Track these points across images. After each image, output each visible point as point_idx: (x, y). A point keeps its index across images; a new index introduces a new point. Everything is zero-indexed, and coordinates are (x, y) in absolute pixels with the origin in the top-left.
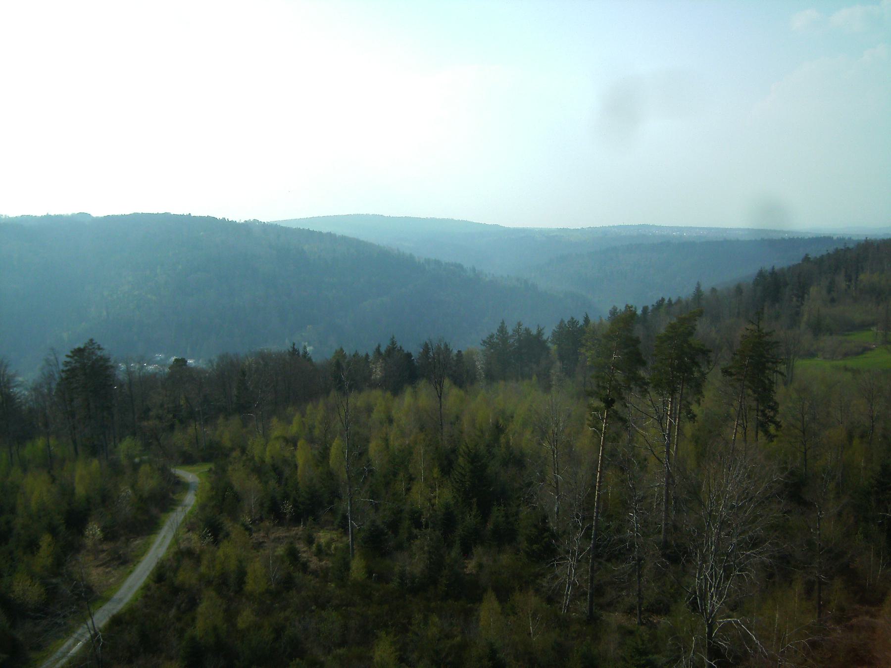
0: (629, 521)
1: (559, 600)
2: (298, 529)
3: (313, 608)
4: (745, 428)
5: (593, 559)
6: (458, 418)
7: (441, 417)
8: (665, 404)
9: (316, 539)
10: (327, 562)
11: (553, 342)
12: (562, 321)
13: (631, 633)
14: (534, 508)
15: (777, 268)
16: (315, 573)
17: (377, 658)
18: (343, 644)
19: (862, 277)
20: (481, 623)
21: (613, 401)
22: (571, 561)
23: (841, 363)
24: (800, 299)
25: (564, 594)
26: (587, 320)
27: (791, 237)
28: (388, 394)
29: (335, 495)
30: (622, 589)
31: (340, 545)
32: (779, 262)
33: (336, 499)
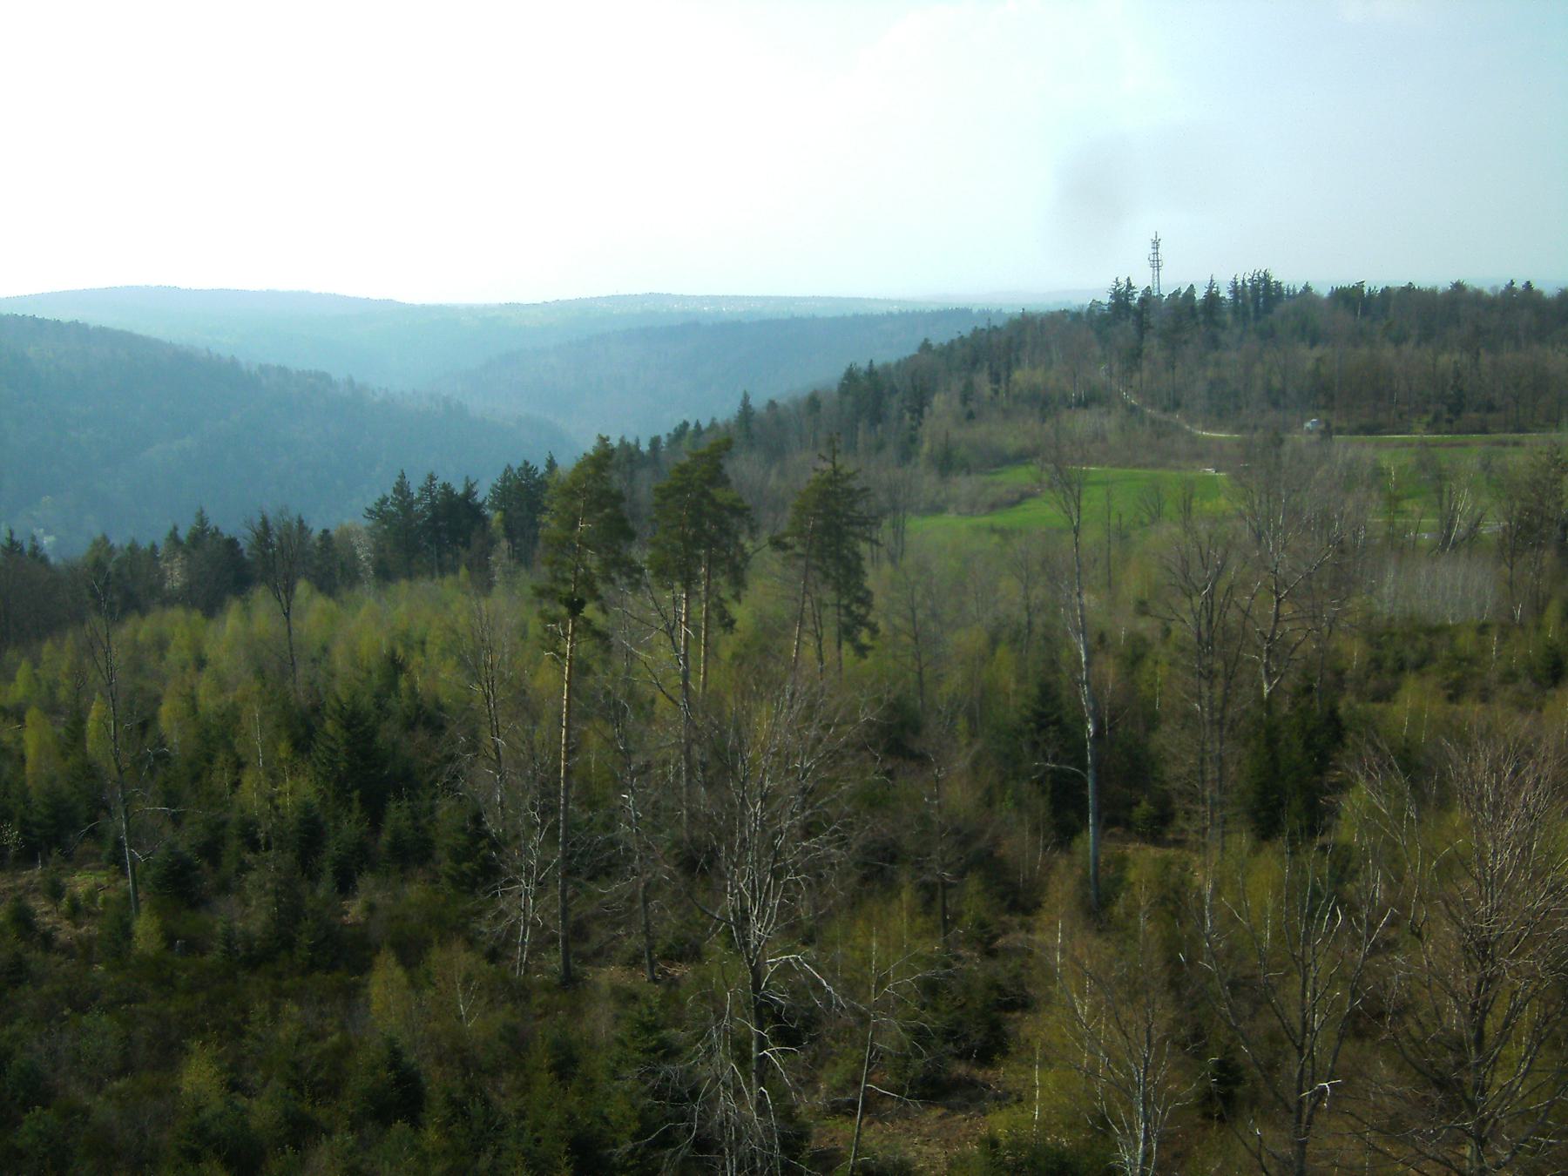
0: (622, 807)
1: (510, 954)
2: (33, 874)
3: (65, 1013)
4: (819, 638)
5: (564, 877)
6: (325, 649)
7: (291, 649)
8: (675, 602)
9: (67, 889)
10: (91, 928)
11: (492, 506)
12: (509, 468)
13: (634, 997)
14: (460, 799)
15: (877, 363)
16: (67, 950)
17: (187, 1088)
18: (126, 1069)
19: (1018, 375)
20: (374, 1007)
21: (582, 603)
22: (525, 885)
23: (985, 520)
24: (916, 415)
25: (517, 943)
26: (551, 465)
27: (904, 311)
28: (197, 616)
29: (100, 806)
30: (619, 925)
31: (112, 895)
32: (887, 353)
33: (103, 813)
